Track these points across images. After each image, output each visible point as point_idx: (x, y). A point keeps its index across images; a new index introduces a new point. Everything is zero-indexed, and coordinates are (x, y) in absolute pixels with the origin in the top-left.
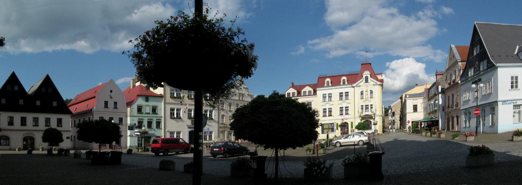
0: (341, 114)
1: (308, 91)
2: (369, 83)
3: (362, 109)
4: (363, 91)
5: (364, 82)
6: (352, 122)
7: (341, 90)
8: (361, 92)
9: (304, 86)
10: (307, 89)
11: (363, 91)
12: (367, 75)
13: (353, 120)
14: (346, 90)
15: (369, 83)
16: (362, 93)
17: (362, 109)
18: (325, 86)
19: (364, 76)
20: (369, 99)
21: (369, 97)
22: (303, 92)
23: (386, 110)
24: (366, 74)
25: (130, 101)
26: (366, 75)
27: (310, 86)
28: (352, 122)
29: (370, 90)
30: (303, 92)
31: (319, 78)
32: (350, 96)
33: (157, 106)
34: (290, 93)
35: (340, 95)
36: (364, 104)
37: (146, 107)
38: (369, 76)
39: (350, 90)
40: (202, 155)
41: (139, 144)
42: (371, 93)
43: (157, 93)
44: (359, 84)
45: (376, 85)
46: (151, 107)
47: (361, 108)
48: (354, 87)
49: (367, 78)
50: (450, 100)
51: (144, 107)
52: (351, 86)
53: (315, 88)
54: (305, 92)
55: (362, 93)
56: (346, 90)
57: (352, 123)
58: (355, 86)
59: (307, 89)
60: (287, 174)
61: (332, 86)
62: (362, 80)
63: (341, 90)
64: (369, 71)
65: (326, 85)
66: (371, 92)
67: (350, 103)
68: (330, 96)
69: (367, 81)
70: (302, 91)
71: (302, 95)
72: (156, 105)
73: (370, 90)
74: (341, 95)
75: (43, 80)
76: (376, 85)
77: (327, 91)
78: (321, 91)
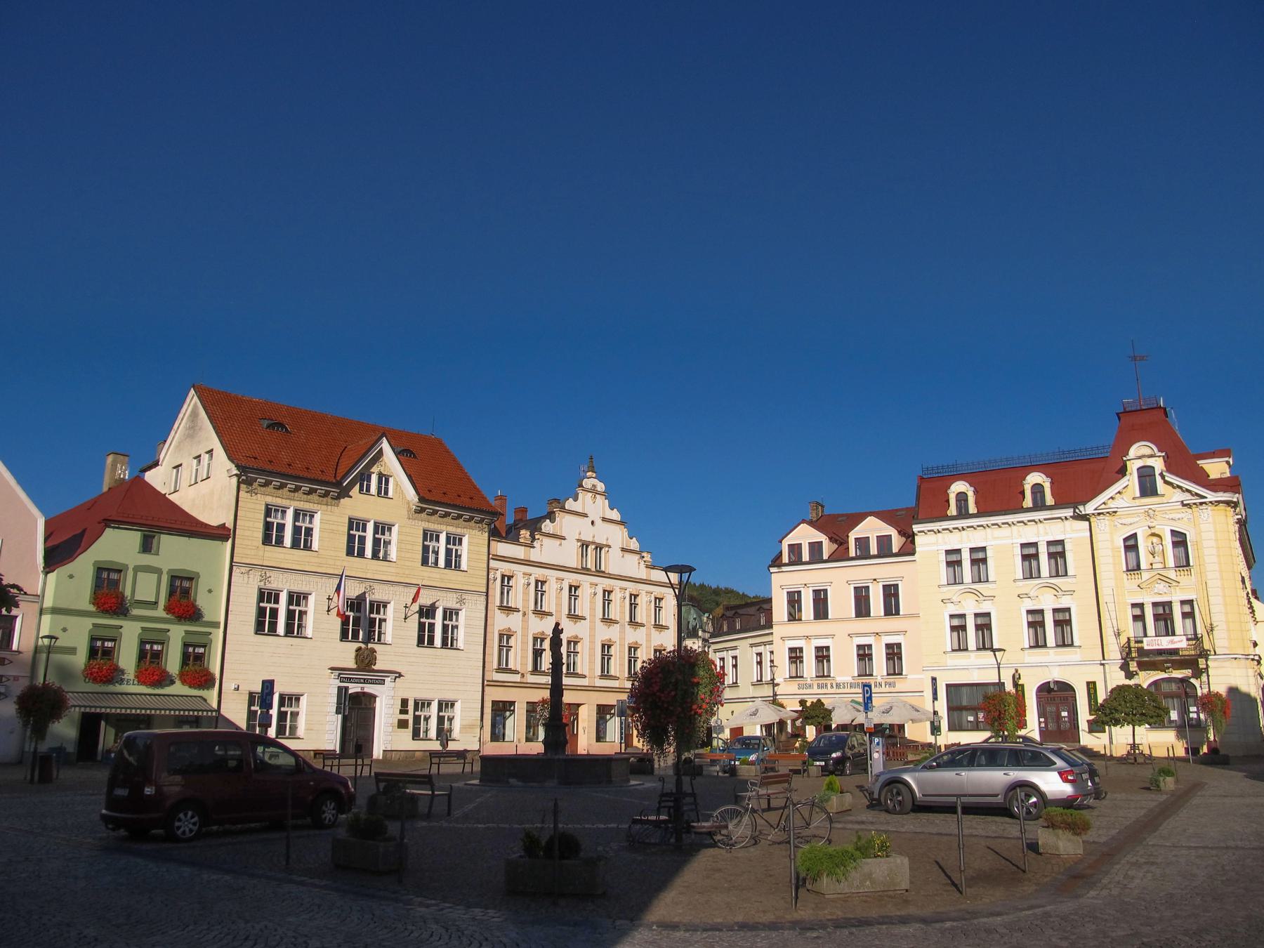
2: (1163, 495)
3: (1139, 618)
4: (1134, 536)
5: (1138, 494)
6: (1094, 683)
7: (1030, 534)
8: (1125, 540)
9: (857, 519)
10: (872, 528)
12: (1150, 462)
13: (1095, 674)
15: (1163, 495)
16: (1131, 545)
17: (1139, 618)
19: (1133, 466)
20: (1172, 574)
21: (1171, 562)
23: (177, 818)
24: (1140, 458)
26: (1140, 463)
27: (885, 517)
28: (1094, 683)
29: (1172, 531)
31: (921, 478)
32: (1076, 559)
33: (94, 564)
35: (1170, 634)
36: (1148, 599)
37: (140, 575)
38: (1158, 464)
39: (1070, 531)
41: (427, 707)
42: (1175, 544)
43: (199, 519)
45: (1201, 504)
46: (165, 578)
47: (1019, 558)
48: (1085, 518)
50: (485, 716)
51: (130, 574)
52: (1069, 512)
53: (904, 521)
55: (1131, 545)
57: (1091, 686)
59: (872, 528)
61: (980, 514)
66: (1180, 541)
68: (979, 558)
69: (1148, 487)
70: (853, 536)
72: (116, 563)
73: (1172, 531)
74: (1029, 555)
76: (1201, 504)
77: (965, 537)
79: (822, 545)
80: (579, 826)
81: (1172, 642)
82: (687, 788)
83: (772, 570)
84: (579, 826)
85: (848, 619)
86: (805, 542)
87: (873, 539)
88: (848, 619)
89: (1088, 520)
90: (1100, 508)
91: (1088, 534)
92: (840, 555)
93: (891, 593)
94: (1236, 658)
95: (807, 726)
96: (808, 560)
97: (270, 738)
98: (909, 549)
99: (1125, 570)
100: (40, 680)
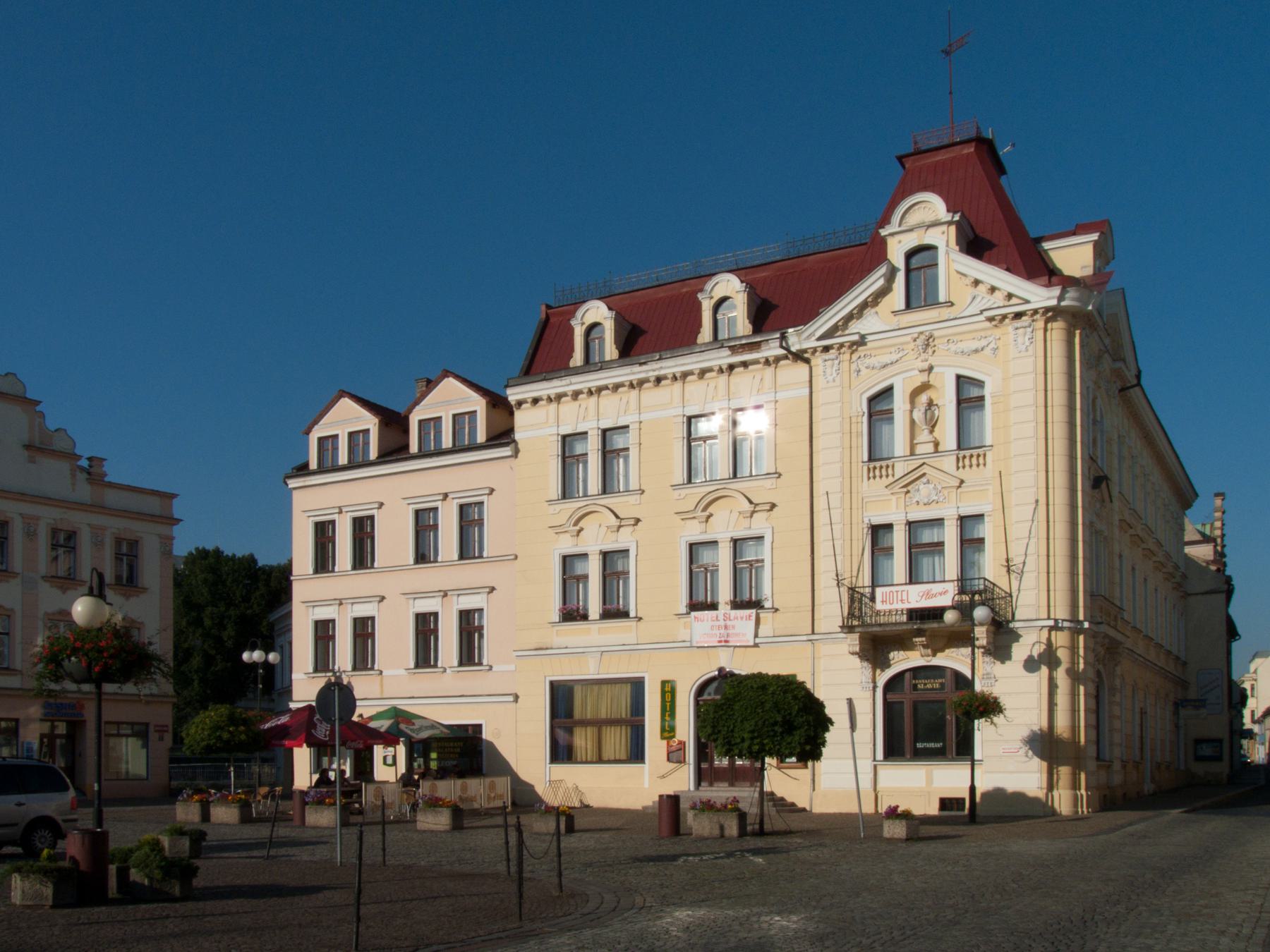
0: (572, 614)
1: (351, 434)
4: (889, 390)
7: (572, 417)
11: (889, 390)
12: (932, 237)
14: (610, 411)
16: (879, 405)
18: (572, 364)
19: (896, 252)
22: (420, 422)
25: (99, 456)
26: (911, 241)
30: (420, 422)
34: (335, 437)
38: (944, 239)
40: (138, 779)
44: (857, 327)
48: (799, 356)
49: (921, 256)
54: (327, 444)
55: (879, 405)
56: (610, 411)
58: (815, 350)
60: (451, 908)
62: (874, 281)
63: (572, 417)
64: (940, 194)
65: (577, 359)
67: (638, 521)
71: (414, 448)
75: (1012, 202)
78: (544, 412)
79: (476, 416)
80: (40, 912)
81: (928, 595)
82: (372, 855)
83: (293, 483)
84: (40, 912)
85: (401, 568)
86: (343, 432)
87: (447, 422)
88: (401, 568)
89: (807, 361)
90: (1021, 302)
91: (807, 391)
92: (394, 450)
93: (470, 519)
94: (566, 648)
95: (375, 747)
96: (450, 445)
97: (128, 778)
98: (502, 435)
99: (866, 459)
100: (937, 559)
